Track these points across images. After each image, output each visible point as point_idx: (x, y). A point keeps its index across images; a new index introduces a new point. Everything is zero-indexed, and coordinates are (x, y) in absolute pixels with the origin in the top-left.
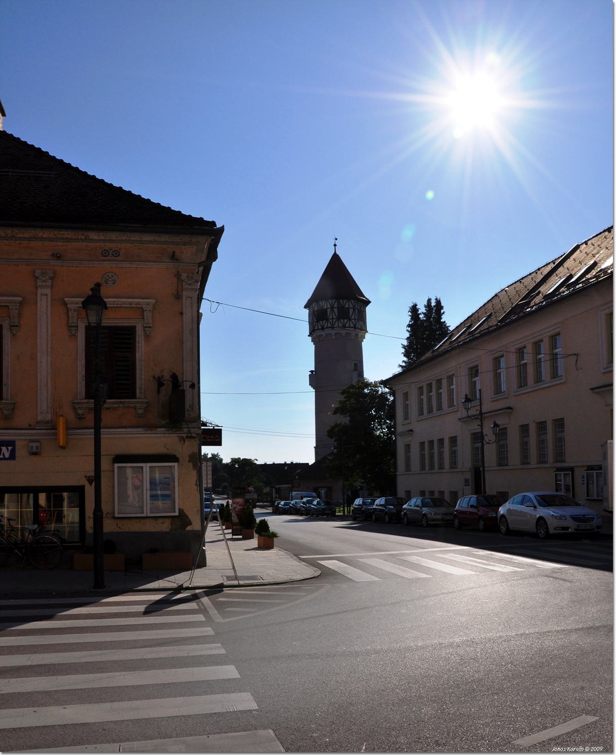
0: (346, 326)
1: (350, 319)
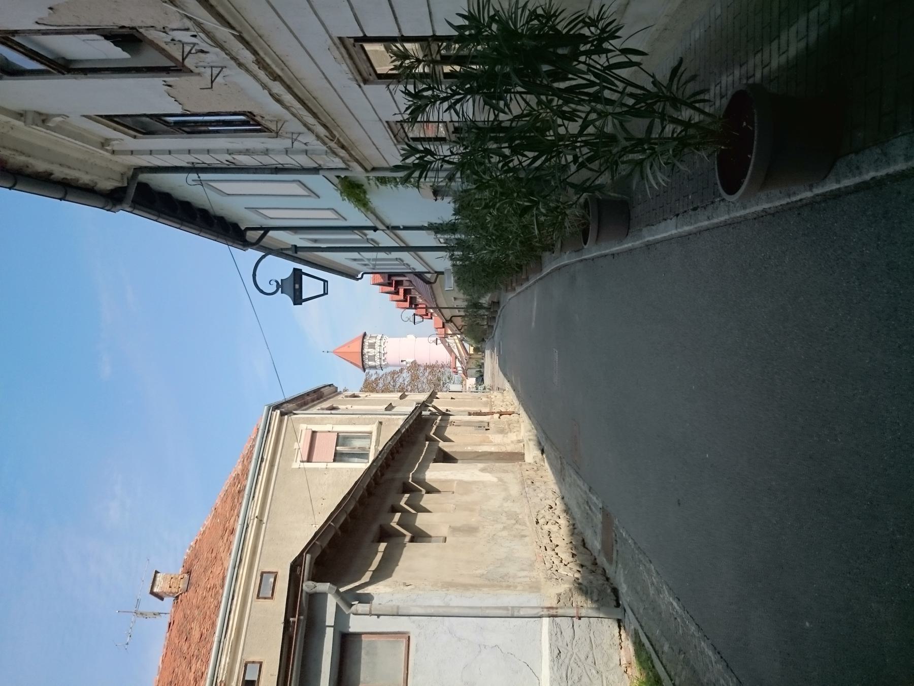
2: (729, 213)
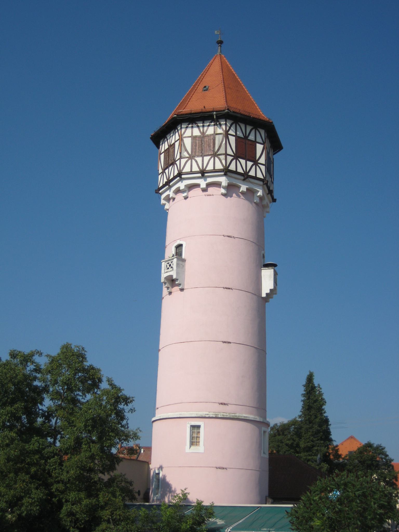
0: (250, 174)
1: (256, 163)
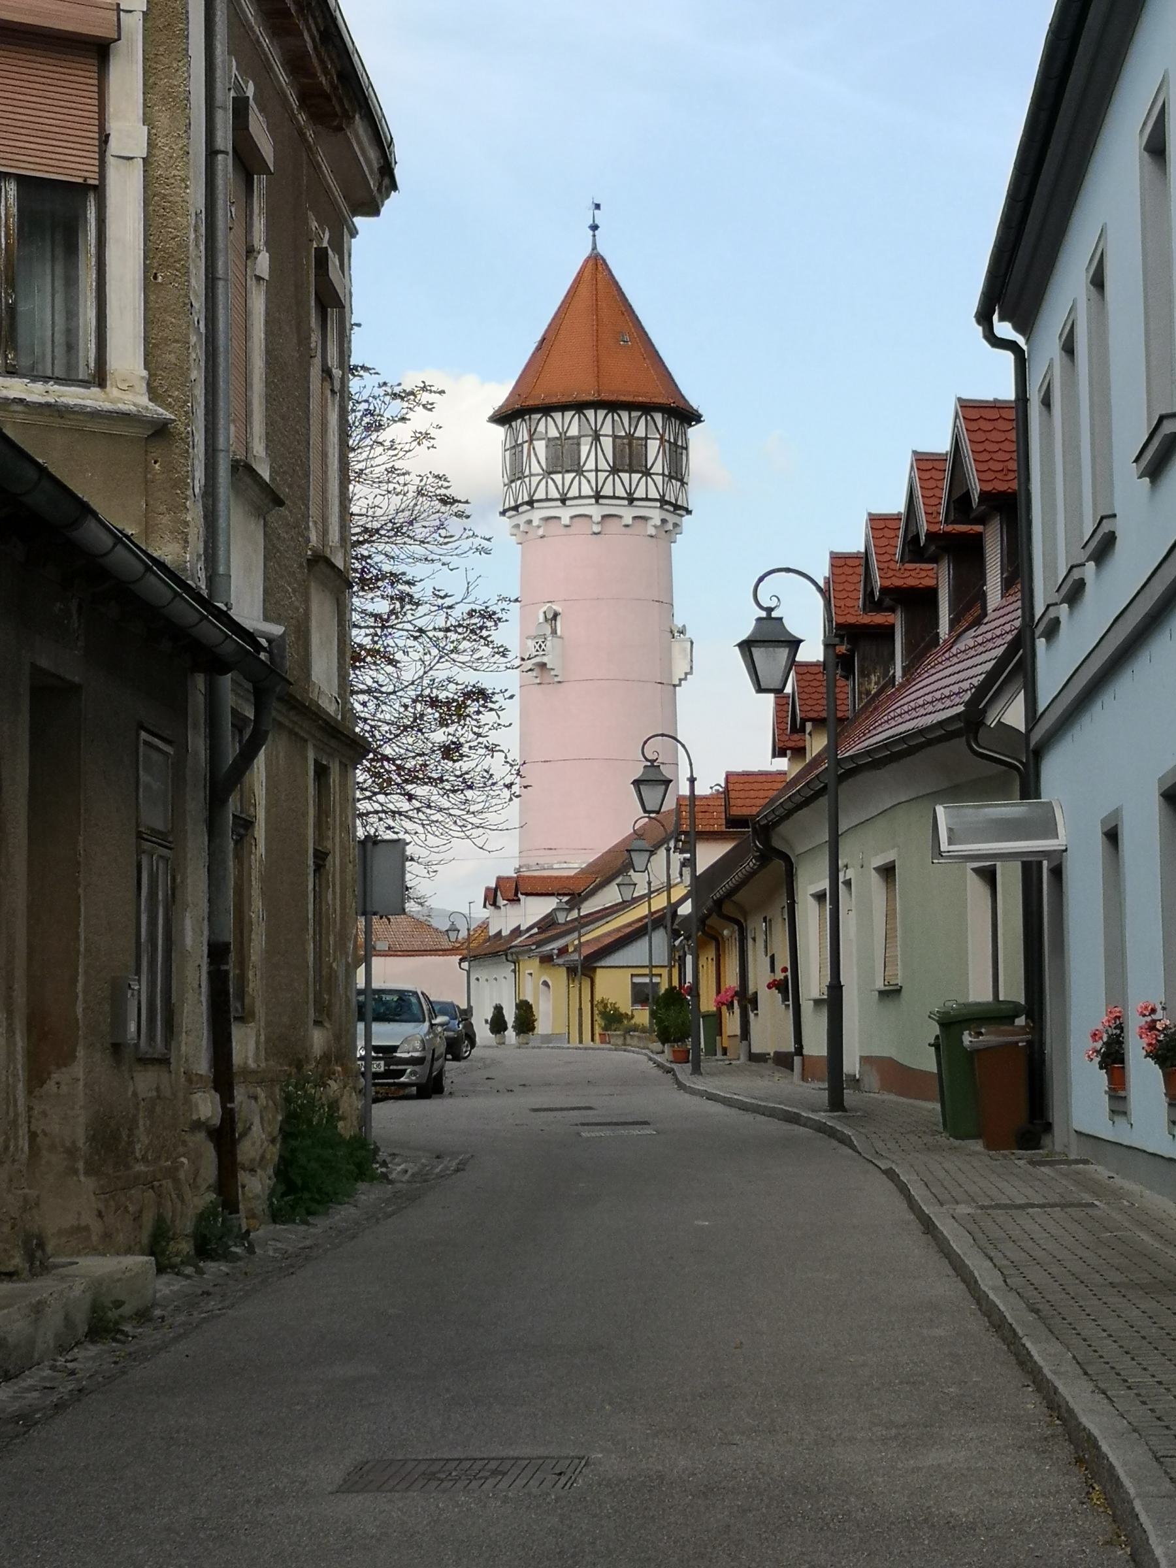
1: (647, 473)
2: (1138, 1495)
